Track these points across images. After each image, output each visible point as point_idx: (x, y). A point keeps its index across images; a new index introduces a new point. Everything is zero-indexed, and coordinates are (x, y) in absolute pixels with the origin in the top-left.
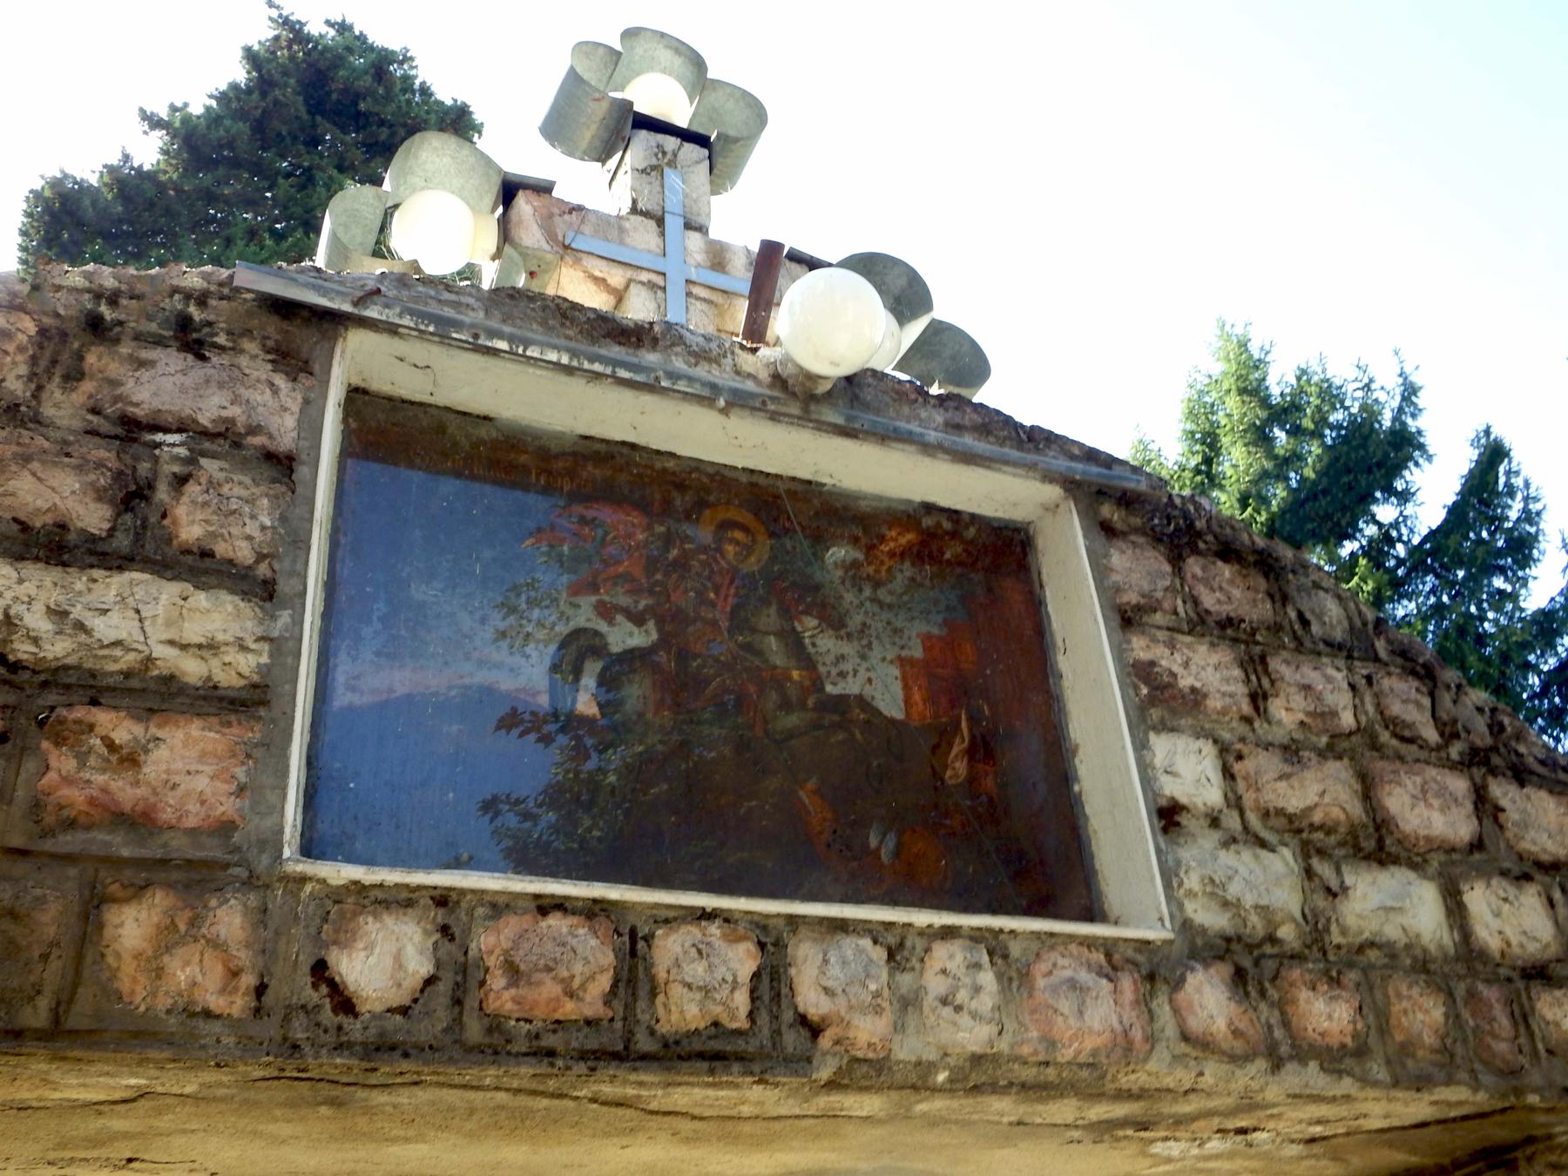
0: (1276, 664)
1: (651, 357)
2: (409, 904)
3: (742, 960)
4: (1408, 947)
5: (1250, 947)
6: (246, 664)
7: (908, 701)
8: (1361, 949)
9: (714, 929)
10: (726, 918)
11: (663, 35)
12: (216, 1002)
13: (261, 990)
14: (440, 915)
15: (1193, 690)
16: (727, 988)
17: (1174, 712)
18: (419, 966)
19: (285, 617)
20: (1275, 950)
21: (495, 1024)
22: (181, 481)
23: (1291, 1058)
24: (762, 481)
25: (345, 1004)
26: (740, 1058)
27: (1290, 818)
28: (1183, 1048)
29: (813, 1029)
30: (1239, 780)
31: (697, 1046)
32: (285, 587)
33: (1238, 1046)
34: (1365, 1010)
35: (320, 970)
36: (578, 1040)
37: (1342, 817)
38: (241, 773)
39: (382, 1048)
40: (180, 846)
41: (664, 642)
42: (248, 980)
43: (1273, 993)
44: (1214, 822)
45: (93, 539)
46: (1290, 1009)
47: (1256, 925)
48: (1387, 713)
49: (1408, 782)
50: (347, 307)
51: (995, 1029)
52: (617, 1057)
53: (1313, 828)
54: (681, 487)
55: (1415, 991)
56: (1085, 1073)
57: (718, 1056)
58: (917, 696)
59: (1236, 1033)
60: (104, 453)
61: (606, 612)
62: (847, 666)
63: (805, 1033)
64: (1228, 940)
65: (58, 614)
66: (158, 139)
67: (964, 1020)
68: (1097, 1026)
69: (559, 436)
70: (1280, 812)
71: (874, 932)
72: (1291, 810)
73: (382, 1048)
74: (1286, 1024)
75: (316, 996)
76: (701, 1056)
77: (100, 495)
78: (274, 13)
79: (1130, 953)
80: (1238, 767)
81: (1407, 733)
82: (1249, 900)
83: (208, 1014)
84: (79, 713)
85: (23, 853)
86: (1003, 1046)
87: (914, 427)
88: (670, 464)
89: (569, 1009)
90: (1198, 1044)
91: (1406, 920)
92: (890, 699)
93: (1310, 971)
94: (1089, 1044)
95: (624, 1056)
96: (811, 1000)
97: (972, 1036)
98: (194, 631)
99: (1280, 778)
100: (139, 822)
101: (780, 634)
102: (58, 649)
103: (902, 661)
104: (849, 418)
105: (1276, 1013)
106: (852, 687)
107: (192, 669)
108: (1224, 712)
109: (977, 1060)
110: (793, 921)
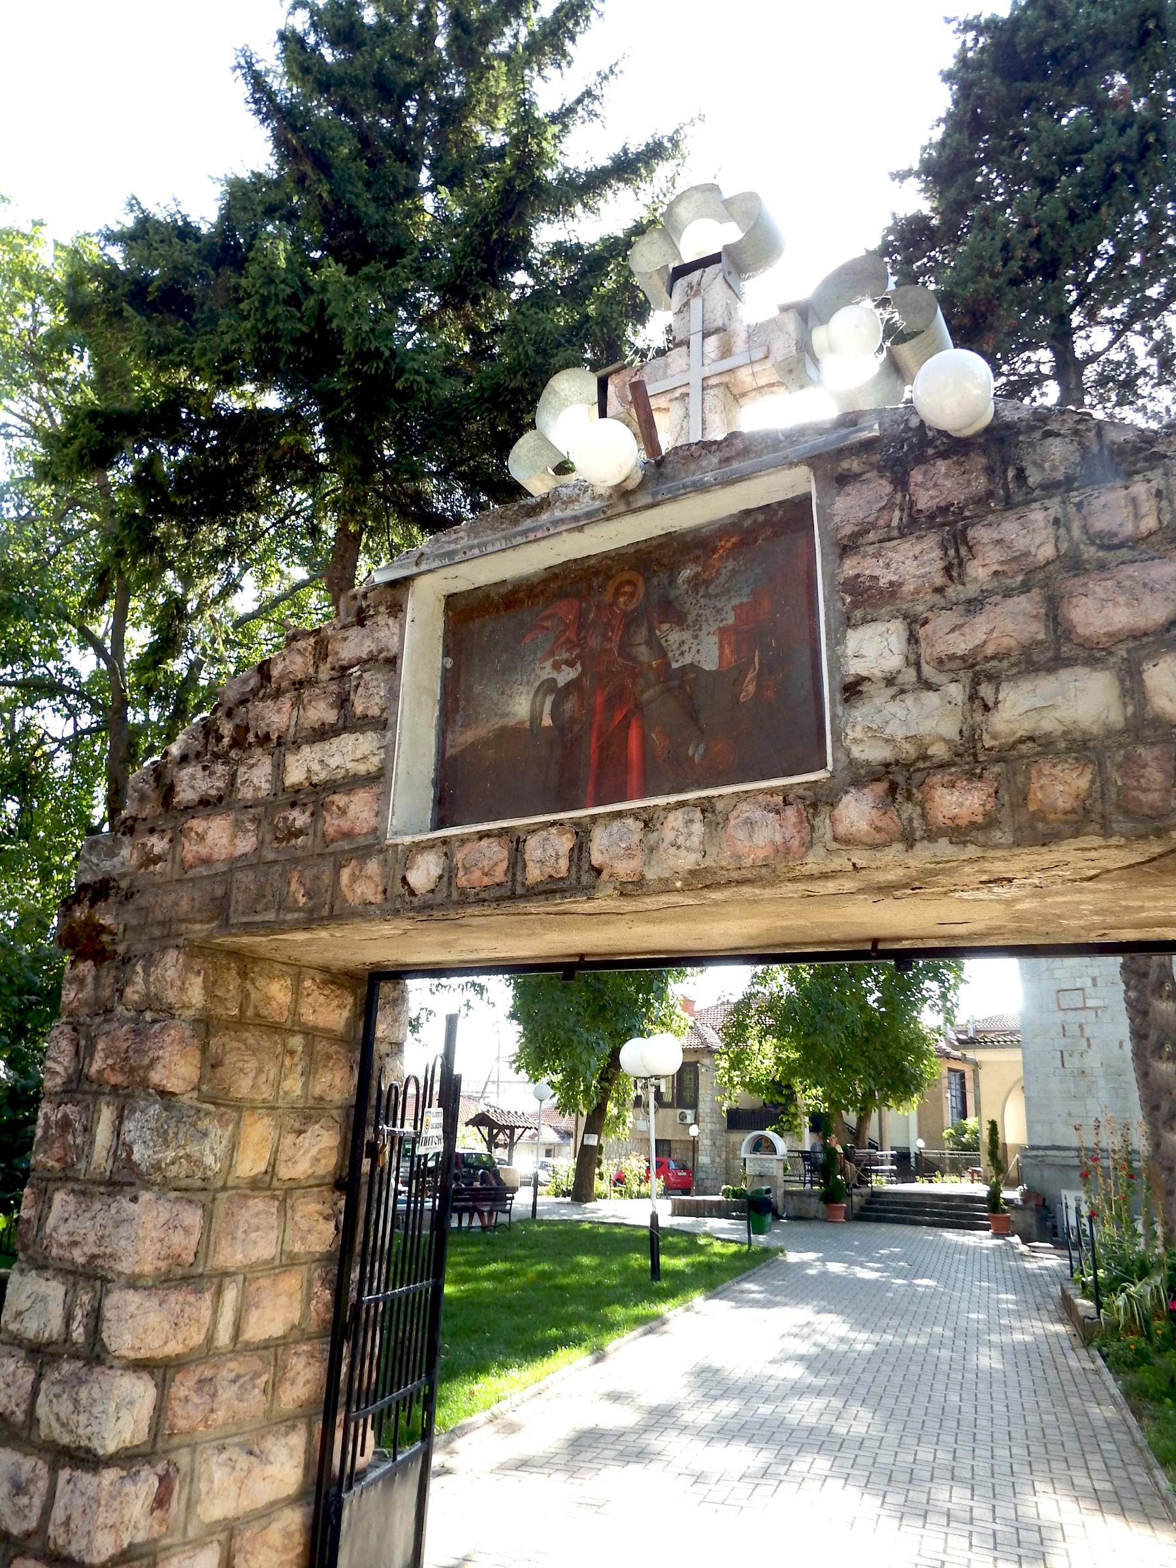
1: (545, 517)
2: (433, 846)
3: (564, 843)
4: (1065, 733)
5: (907, 766)
8: (1013, 746)
9: (553, 830)
10: (560, 823)
11: (695, 188)
12: (372, 899)
13: (385, 891)
14: (444, 849)
15: (891, 583)
16: (553, 860)
17: (874, 607)
18: (436, 871)
19: (389, 734)
20: (928, 764)
21: (462, 892)
23: (923, 838)
24: (642, 546)
25: (412, 893)
26: (563, 891)
27: (963, 658)
28: (835, 845)
29: (599, 871)
30: (923, 643)
31: (541, 888)
32: (390, 721)
33: (880, 838)
34: (1001, 792)
35: (404, 879)
36: (493, 893)
37: (1013, 643)
38: (376, 807)
39: (427, 907)
40: (362, 841)
42: (380, 888)
43: (918, 795)
45: (332, 725)
46: (927, 805)
47: (910, 751)
48: (1091, 531)
49: (1098, 589)
50: (415, 570)
51: (700, 856)
52: (509, 898)
53: (987, 659)
54: (596, 574)
55: (1057, 771)
56: (764, 871)
57: (553, 892)
58: (727, 651)
59: (878, 829)
61: (557, 667)
62: (685, 647)
63: (594, 874)
64: (888, 765)
66: (914, 184)
67: (683, 852)
68: (761, 843)
69: (535, 574)
70: (952, 657)
71: (635, 814)
72: (960, 653)
73: (427, 907)
74: (923, 816)
76: (545, 892)
77: (332, 706)
78: (954, 25)
79: (801, 792)
80: (922, 632)
81: (1116, 541)
82: (900, 734)
83: (371, 903)
85: (320, 855)
86: (708, 862)
88: (593, 561)
89: (487, 881)
90: (847, 841)
91: (1058, 714)
93: (951, 774)
94: (761, 854)
95: (513, 897)
96: (597, 858)
97: (687, 861)
99: (953, 630)
100: (348, 835)
101: (648, 643)
104: (654, 495)
105: (918, 810)
107: (362, 768)
108: (917, 591)
109: (692, 872)
110: (594, 818)
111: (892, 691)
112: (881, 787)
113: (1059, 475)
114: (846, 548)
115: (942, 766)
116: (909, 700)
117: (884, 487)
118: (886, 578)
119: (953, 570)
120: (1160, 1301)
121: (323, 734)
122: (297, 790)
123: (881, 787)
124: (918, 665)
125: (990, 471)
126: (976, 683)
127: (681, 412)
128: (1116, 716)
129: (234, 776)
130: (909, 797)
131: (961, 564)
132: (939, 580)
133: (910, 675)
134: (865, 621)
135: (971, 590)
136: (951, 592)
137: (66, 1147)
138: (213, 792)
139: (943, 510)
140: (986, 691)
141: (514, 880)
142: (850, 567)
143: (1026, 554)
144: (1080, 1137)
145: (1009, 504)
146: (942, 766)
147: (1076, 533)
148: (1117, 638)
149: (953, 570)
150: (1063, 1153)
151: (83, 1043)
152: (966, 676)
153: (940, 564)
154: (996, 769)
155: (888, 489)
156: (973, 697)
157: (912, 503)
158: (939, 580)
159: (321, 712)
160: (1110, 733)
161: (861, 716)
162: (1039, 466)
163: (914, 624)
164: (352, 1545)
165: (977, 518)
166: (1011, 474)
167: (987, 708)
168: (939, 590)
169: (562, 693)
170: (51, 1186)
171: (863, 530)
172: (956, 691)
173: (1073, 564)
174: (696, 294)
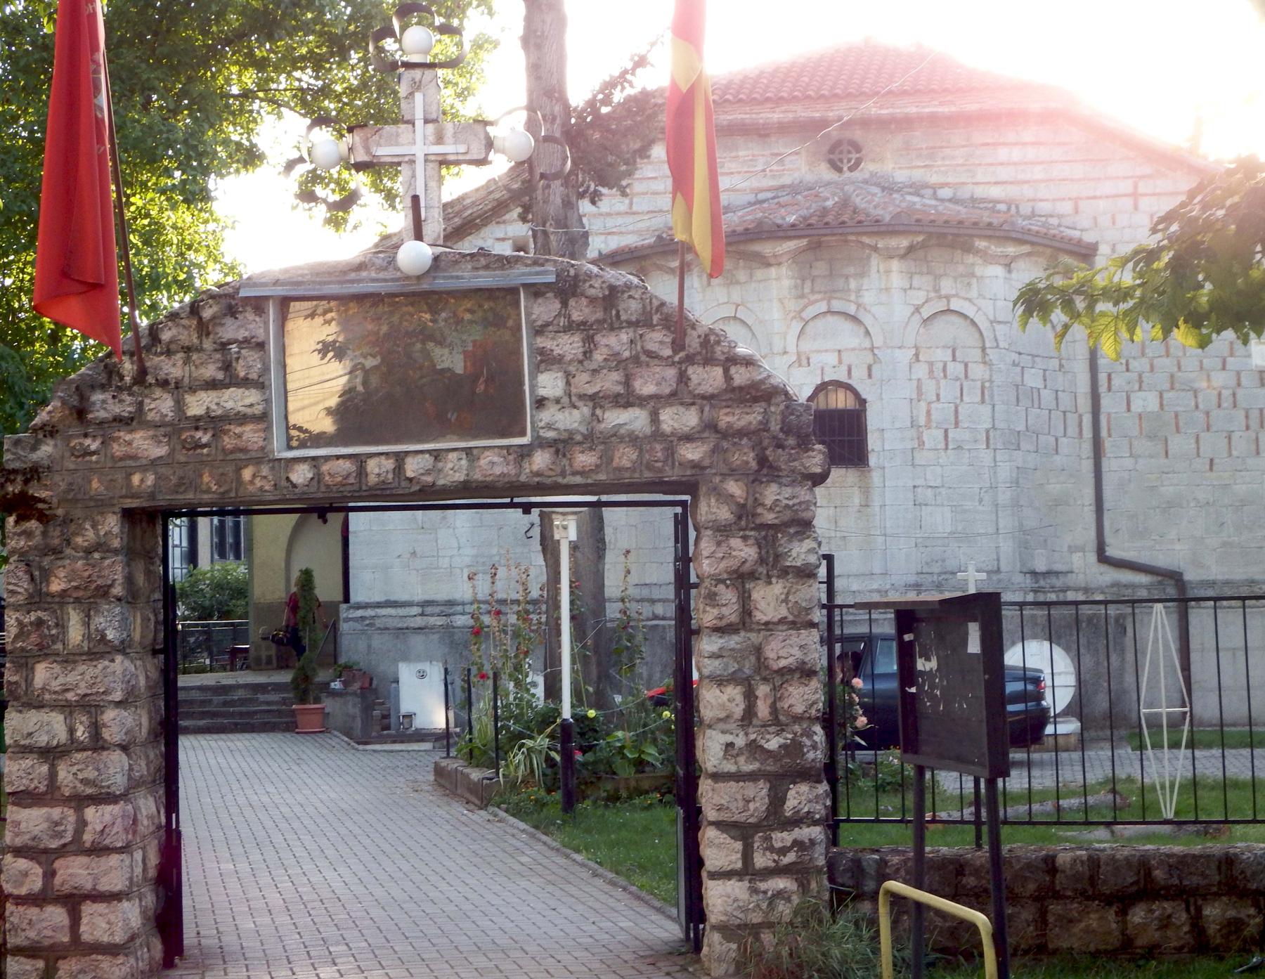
0: (598, 338)
3: (389, 464)
6: (258, 410)
7: (465, 367)
22: (238, 359)
25: (295, 486)
32: (267, 383)
35: (288, 478)
40: (254, 454)
41: (383, 360)
44: (558, 401)
60: (218, 356)
65: (218, 404)
71: (429, 452)
75: (288, 484)
77: (220, 369)
80: (572, 381)
84: (227, 427)
87: (460, 274)
92: (459, 368)
98: (247, 401)
102: (219, 412)
103: (465, 353)
106: (446, 365)
107: (249, 411)
111: (559, 406)
112: (552, 450)
113: (634, 319)
114: (539, 331)
115: (580, 443)
116: (567, 412)
117: (557, 305)
118: (557, 351)
119: (587, 354)
120: (532, 771)
121: (212, 385)
122: (197, 419)
123: (552, 450)
124: (570, 396)
125: (605, 309)
126: (594, 408)
127: (410, 173)
128: (648, 430)
129: (141, 404)
130: (564, 455)
131: (591, 352)
132: (581, 357)
133: (565, 400)
134: (547, 370)
135: (594, 366)
136: (586, 363)
137: (42, 636)
138: (126, 415)
139: (584, 323)
140: (598, 412)
141: (360, 482)
142: (541, 342)
143: (618, 354)
144: (474, 587)
145: (612, 329)
146: (580, 443)
147: (639, 348)
148: (651, 397)
149: (587, 354)
150: (401, 611)
151: (37, 573)
152: (591, 404)
153: (581, 350)
154: (601, 447)
155: (559, 306)
156: (593, 414)
157: (570, 316)
158: (581, 357)
159: (211, 371)
160: (646, 437)
161: (546, 416)
162: (626, 311)
163: (568, 377)
164: (145, 870)
165: (598, 331)
166: (614, 312)
167: (599, 421)
168: (581, 362)
169: (367, 373)
170: (31, 661)
171: (547, 324)
172: (586, 410)
173: (635, 359)
174: (418, 89)
